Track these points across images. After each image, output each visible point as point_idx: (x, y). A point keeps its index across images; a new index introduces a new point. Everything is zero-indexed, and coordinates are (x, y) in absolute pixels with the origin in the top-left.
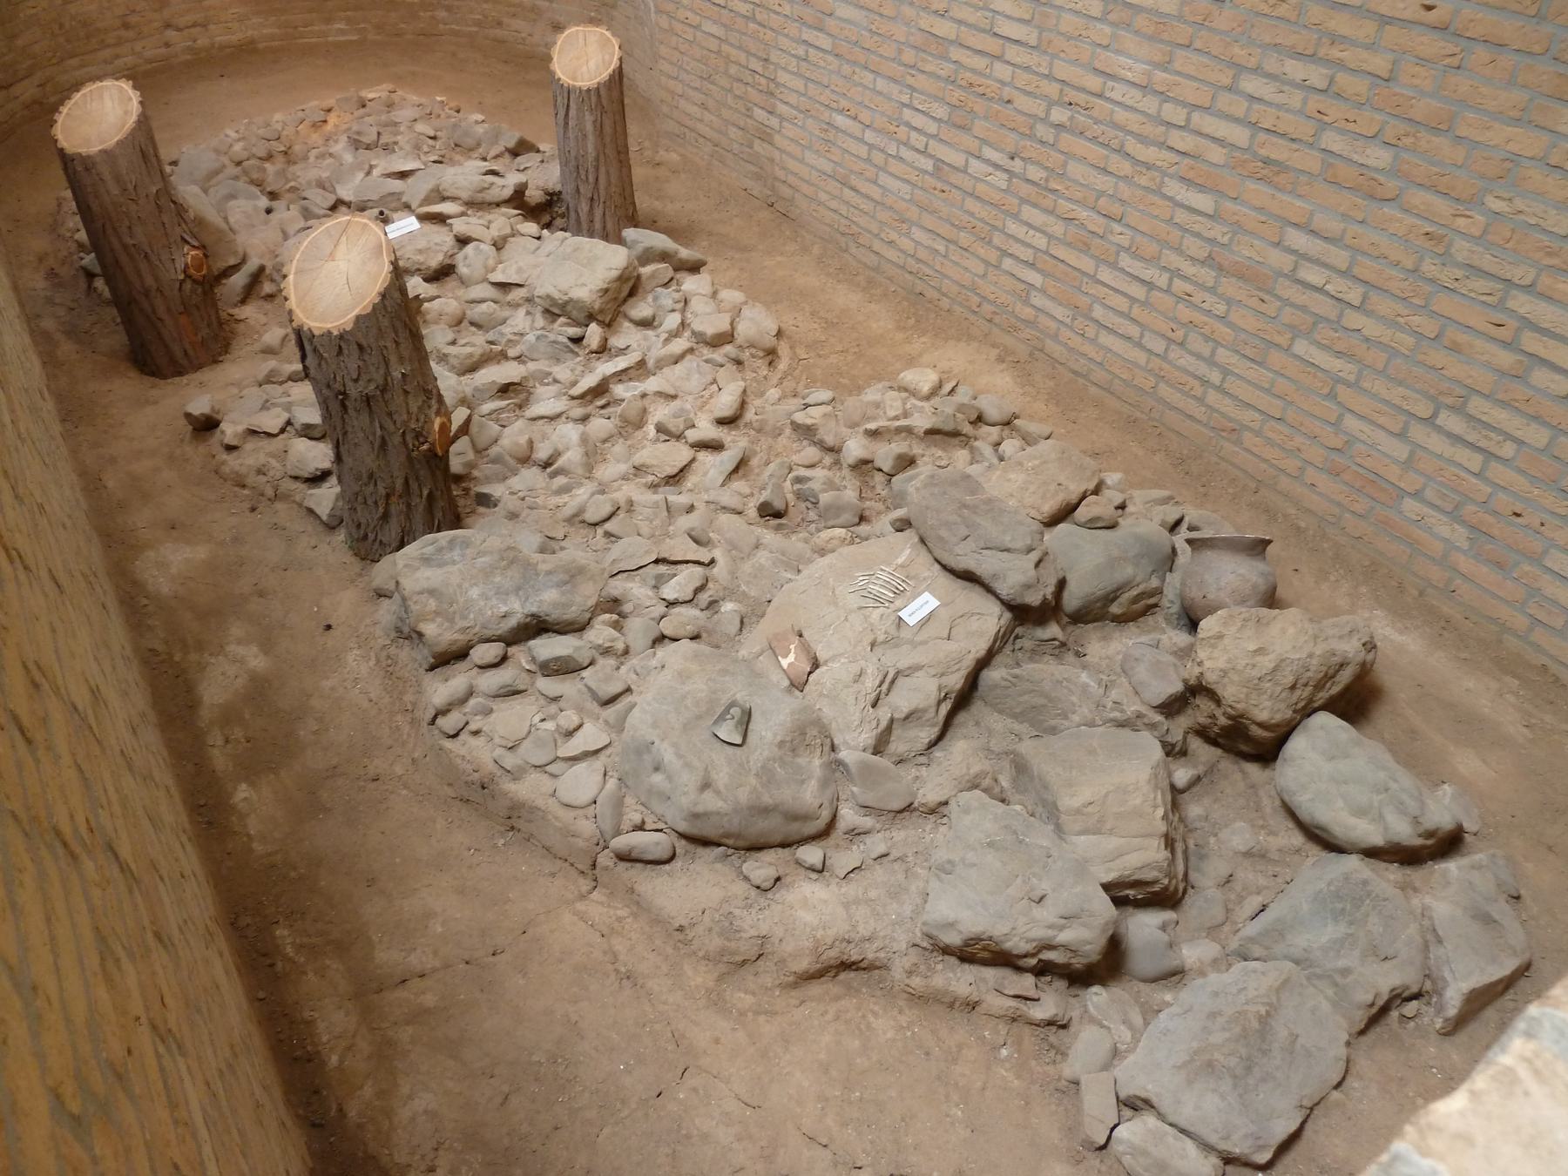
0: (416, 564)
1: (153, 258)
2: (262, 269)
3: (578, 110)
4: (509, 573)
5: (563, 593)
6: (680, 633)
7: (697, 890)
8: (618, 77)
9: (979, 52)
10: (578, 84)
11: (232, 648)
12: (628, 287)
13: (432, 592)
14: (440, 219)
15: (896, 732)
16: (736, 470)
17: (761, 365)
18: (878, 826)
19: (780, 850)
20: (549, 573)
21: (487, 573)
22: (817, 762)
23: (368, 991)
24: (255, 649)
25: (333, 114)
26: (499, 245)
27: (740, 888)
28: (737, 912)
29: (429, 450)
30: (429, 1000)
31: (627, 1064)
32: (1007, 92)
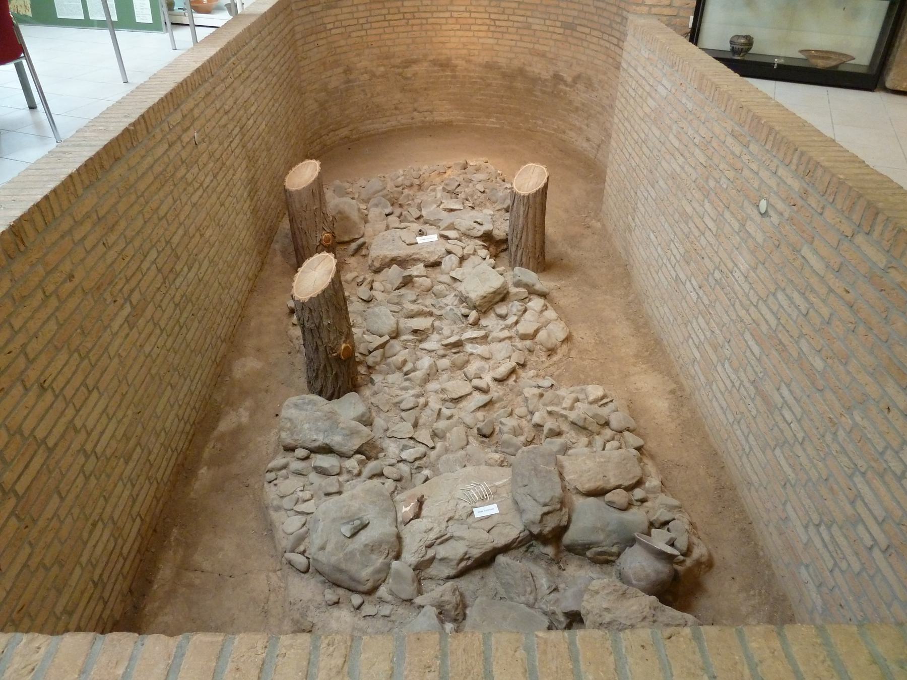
2: (364, 243)
11: (241, 410)
12: (502, 296)
13: (290, 420)
14: (447, 238)
15: (435, 564)
16: (485, 405)
18: (393, 602)
20: (343, 428)
21: (317, 420)
22: (381, 560)
23: (185, 566)
26: (462, 259)
27: (319, 598)
28: (312, 607)
30: (197, 582)
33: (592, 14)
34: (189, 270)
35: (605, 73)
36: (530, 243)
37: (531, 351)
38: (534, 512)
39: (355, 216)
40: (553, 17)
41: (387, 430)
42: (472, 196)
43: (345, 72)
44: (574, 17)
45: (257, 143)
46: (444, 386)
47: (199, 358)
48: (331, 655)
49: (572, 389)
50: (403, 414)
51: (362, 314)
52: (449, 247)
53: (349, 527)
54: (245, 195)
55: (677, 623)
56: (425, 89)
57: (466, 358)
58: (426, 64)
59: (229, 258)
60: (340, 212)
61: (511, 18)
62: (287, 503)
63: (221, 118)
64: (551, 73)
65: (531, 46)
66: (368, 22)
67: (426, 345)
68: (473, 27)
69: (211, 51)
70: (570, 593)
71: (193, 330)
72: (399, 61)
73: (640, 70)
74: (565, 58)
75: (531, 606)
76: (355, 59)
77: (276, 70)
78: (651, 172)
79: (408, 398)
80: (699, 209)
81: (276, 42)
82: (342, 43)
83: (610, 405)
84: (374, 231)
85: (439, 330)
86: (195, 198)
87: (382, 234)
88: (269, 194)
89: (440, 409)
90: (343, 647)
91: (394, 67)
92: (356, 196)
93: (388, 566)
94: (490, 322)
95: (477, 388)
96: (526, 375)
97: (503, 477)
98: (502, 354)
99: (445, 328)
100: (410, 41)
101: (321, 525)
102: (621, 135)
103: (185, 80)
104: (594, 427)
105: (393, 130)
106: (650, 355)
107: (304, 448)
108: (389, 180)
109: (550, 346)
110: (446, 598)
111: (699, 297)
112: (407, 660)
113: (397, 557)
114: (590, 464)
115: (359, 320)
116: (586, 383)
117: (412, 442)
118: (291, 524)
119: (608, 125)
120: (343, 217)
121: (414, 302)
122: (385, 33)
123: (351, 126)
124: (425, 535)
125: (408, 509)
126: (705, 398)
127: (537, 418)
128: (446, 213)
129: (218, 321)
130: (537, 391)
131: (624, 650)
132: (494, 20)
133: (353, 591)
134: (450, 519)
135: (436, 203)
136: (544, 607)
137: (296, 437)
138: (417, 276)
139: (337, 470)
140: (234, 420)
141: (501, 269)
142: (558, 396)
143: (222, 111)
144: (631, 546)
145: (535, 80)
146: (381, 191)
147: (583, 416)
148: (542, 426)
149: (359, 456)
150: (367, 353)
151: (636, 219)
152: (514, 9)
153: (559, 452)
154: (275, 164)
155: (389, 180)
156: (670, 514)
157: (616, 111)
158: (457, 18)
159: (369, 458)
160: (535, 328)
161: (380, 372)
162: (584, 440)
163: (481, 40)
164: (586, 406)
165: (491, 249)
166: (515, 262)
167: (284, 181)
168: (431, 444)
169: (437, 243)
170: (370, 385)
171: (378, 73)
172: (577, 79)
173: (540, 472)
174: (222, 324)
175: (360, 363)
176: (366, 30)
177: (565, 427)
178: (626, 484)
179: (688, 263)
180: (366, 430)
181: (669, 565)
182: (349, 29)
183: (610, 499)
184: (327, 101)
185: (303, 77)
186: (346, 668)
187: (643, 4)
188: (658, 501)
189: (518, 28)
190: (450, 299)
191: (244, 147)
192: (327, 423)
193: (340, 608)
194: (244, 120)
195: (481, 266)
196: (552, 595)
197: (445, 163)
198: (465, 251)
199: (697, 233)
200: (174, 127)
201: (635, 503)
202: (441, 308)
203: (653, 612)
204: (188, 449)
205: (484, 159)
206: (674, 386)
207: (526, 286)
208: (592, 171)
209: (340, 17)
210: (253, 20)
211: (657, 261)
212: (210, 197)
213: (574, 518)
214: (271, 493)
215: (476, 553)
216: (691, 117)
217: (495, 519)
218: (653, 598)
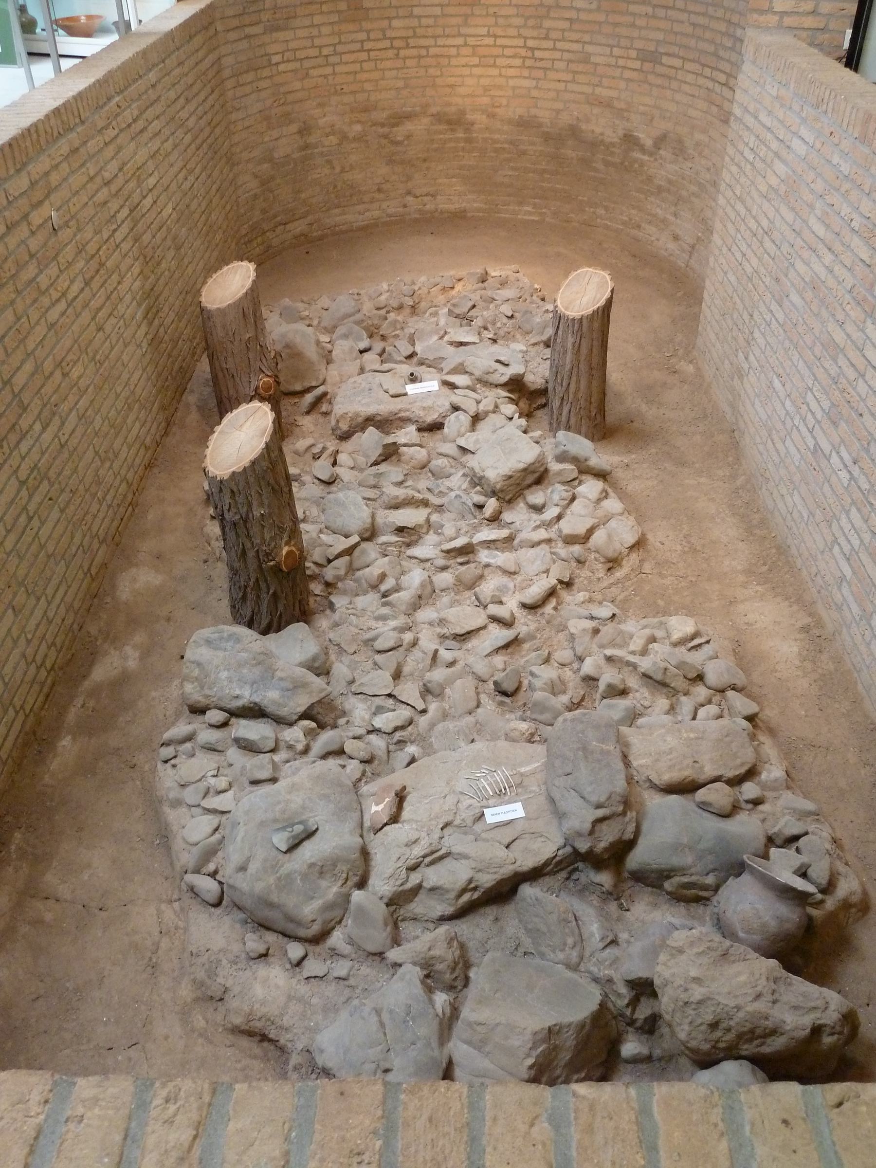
0: (202, 643)
1: (237, 380)
2: (325, 394)
3: (564, 331)
5: (283, 696)
7: (215, 933)
8: (605, 313)
9: (853, 365)
10: (567, 313)
11: (128, 650)
12: (536, 476)
13: (199, 664)
14: (452, 386)
16: (507, 646)
17: (600, 570)
19: (281, 937)
20: (281, 679)
21: (240, 665)
22: (335, 889)
24: (137, 654)
25: (461, 283)
26: (476, 419)
27: (236, 948)
28: (224, 962)
29: (275, 566)
30: (48, 917)
31: (109, 1019)
32: (862, 408)
33: (686, 35)
34: (44, 429)
35: (704, 131)
37: (580, 562)
38: (581, 817)
39: (311, 352)
40: (624, 42)
41: (353, 682)
42: (494, 323)
43: (300, 132)
44: (658, 41)
46: (443, 614)
48: (169, 1122)
49: (644, 622)
50: (379, 658)
51: (318, 501)
52: (457, 398)
53: (285, 835)
54: (139, 315)
55: (813, 1004)
56: (425, 160)
57: (479, 571)
58: (426, 120)
59: (113, 413)
60: (287, 346)
61: (559, 45)
62: (190, 795)
63: (97, 191)
64: (621, 133)
65: (588, 89)
66: (336, 53)
67: (417, 551)
68: (499, 61)
69: (80, 84)
70: (636, 948)
71: (50, 525)
72: (384, 115)
73: (763, 117)
74: (642, 108)
75: (574, 968)
76: (317, 112)
77: (191, 123)
78: (778, 280)
79: (387, 633)
80: (856, 335)
81: (190, 79)
82: (298, 85)
83: (706, 648)
84: (341, 375)
85: (438, 529)
86: (53, 315)
87: (352, 380)
88: (180, 317)
89: (436, 651)
90: (195, 1106)
91: (375, 124)
92: (315, 323)
93: (347, 898)
94: (518, 516)
95: (495, 619)
96: (572, 599)
97: (532, 760)
99: (447, 525)
100: (400, 84)
101: (241, 831)
102: (730, 226)
103: (35, 125)
104: (679, 683)
105: (376, 225)
106: (770, 570)
107: (221, 709)
108: (365, 298)
109: (611, 554)
110: (436, 952)
111: (852, 478)
112: (317, 1137)
113: (362, 884)
114: (672, 741)
115: (314, 511)
116: (666, 613)
117: (391, 701)
118: (196, 829)
119: (708, 213)
120: (293, 353)
121: (400, 484)
122: (362, 70)
123: (310, 219)
124: (408, 850)
126: (858, 639)
127: (588, 667)
128: (452, 349)
129: (94, 509)
130: (589, 624)
131: (747, 1128)
132: (532, 49)
133: (289, 937)
135: (436, 332)
136: (595, 970)
137: (207, 692)
138: (405, 445)
139: (271, 745)
140: (115, 665)
141: (537, 434)
142: (621, 632)
143: (98, 180)
144: (738, 875)
145: (595, 145)
147: (663, 665)
148: (596, 680)
149: (306, 723)
150: (325, 563)
151: (752, 358)
152: (563, 30)
153: (621, 722)
154: (190, 270)
155: (365, 298)
156: (801, 823)
157: (723, 186)
158: (474, 46)
159: (322, 726)
160: (588, 526)
161: (345, 592)
162: (663, 703)
163: (511, 83)
164: (667, 648)
165: (521, 404)
166: (559, 424)
167: (199, 292)
168: (420, 706)
169: (437, 395)
170: (328, 612)
171: (351, 135)
172: (661, 140)
173: (592, 752)
174: (101, 515)
175: (313, 577)
176: (333, 65)
177: (633, 682)
178: (730, 774)
179: (834, 423)
180: (319, 682)
181: (798, 910)
182: (307, 64)
183: (703, 799)
184: (273, 178)
185: (236, 139)
186: (197, 1152)
187: (770, 11)
188: (781, 803)
189: (570, 61)
190: (457, 481)
191: (136, 240)
192: (257, 671)
193: (268, 964)
194: (136, 197)
195: (506, 429)
196: (608, 951)
197: (452, 273)
198: (481, 407)
199: (851, 374)
200: (16, 198)
201: (743, 805)
202: (441, 494)
203: (774, 987)
205: (514, 267)
206: (808, 620)
207: (575, 460)
208: (683, 287)
209: (292, 45)
210: (150, 40)
211: (784, 423)
212: (78, 316)
213: (645, 827)
214: (167, 779)
215: (487, 880)
216: (846, 186)
218: (773, 962)
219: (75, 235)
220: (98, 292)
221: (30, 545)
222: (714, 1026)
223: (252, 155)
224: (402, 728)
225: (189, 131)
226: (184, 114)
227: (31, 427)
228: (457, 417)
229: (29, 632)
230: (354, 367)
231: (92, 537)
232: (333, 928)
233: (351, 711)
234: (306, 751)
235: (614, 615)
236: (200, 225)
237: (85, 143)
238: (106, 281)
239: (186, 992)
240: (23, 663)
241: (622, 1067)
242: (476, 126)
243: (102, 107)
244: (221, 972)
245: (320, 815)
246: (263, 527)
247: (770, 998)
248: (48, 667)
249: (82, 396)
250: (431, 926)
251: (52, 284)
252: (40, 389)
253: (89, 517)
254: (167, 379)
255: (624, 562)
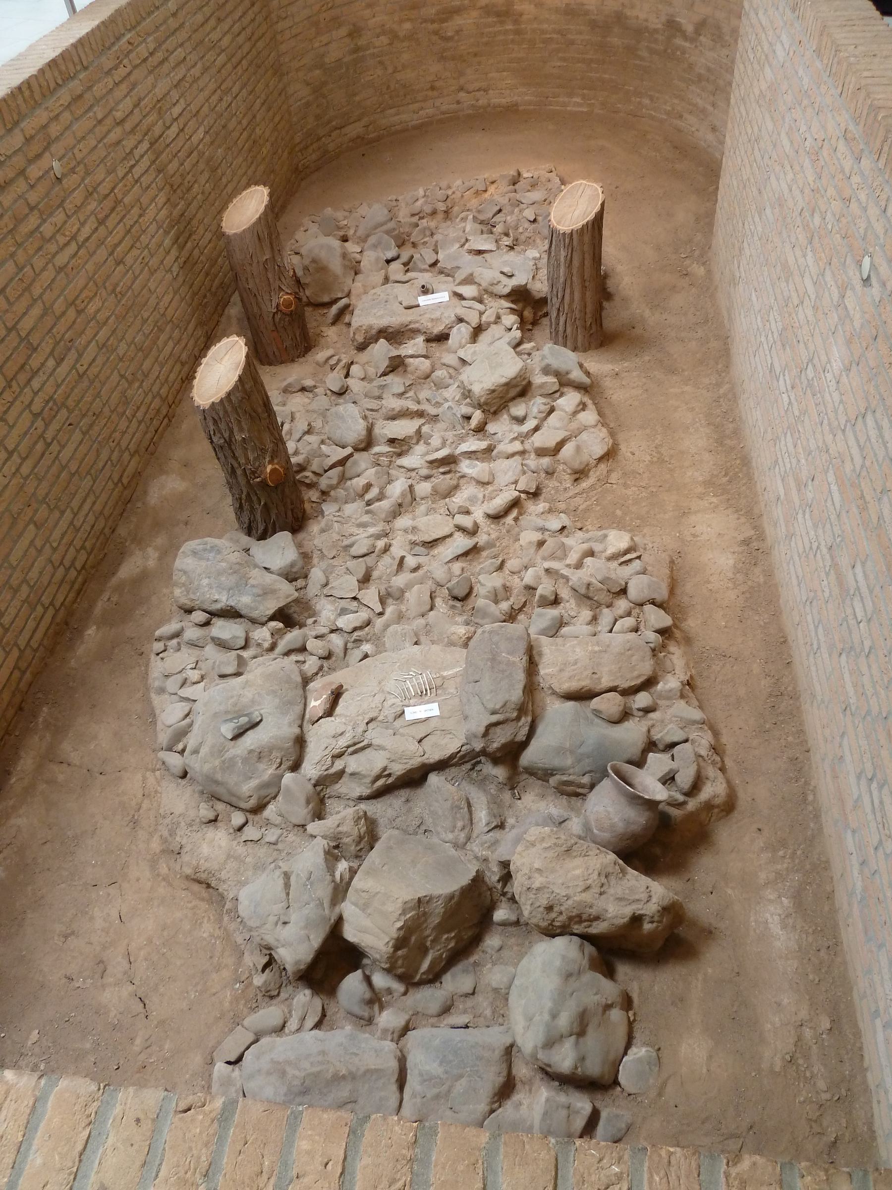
1: (259, 298)
3: (557, 245)
4: (231, 578)
5: (254, 601)
6: (315, 652)
7: (178, 800)
10: (559, 227)
11: (150, 550)
12: (519, 389)
13: (185, 572)
14: (461, 297)
15: (345, 779)
16: (466, 554)
20: (253, 586)
21: (220, 573)
23: (51, 756)
25: (495, 185)
26: (478, 331)
28: (183, 824)
30: (61, 778)
36: (577, 305)
39: (336, 265)
43: (350, 35)
45: (187, 165)
47: (87, 482)
53: (232, 725)
54: (167, 242)
55: (637, 897)
56: (475, 55)
57: (455, 482)
58: (475, 14)
60: (314, 261)
63: (109, 131)
64: (664, 19)
67: (405, 461)
72: (434, 11)
77: (226, 41)
89: (402, 558)
91: (425, 21)
94: (501, 427)
97: (454, 664)
98: (507, 477)
103: (28, 83)
106: (730, 481)
107: (204, 611)
109: (577, 465)
113: (295, 767)
117: (355, 603)
120: (318, 267)
121: (401, 395)
123: (365, 121)
125: (317, 703)
128: (469, 257)
129: (123, 425)
130: (537, 536)
134: (371, 720)
136: (476, 849)
137: (192, 596)
138: (412, 356)
143: (109, 121)
145: (639, 32)
146: (385, 223)
149: (274, 624)
160: (559, 439)
161: (336, 500)
162: (587, 614)
172: (700, 26)
178: (625, 685)
183: (595, 707)
184: (324, 84)
185: (283, 48)
188: (670, 711)
190: (452, 392)
191: (159, 171)
192: (233, 579)
193: (217, 828)
196: (491, 834)
201: (635, 713)
204: (74, 602)
215: (398, 769)
217: (432, 724)
219: (83, 179)
220: (115, 228)
221: (49, 467)
222: (550, 908)
223: (301, 63)
224: (361, 628)
225: (223, 51)
226: (215, 36)
227: (43, 364)
228: (459, 329)
229: (55, 541)
230: (379, 277)
231: (122, 452)
232: (269, 802)
233: (320, 612)
234: (272, 648)
235: (563, 528)
236: (240, 143)
237: (90, 88)
238: (124, 216)
239: (156, 845)
240: (49, 568)
241: (494, 928)
242: (525, 17)
243: (109, 49)
244: (179, 832)
245: (267, 708)
246: (246, 449)
247: (597, 890)
248: (79, 568)
249: (101, 328)
250: (352, 803)
251: (58, 231)
252: (52, 328)
253: (117, 435)
254: (205, 296)
255: (591, 473)
